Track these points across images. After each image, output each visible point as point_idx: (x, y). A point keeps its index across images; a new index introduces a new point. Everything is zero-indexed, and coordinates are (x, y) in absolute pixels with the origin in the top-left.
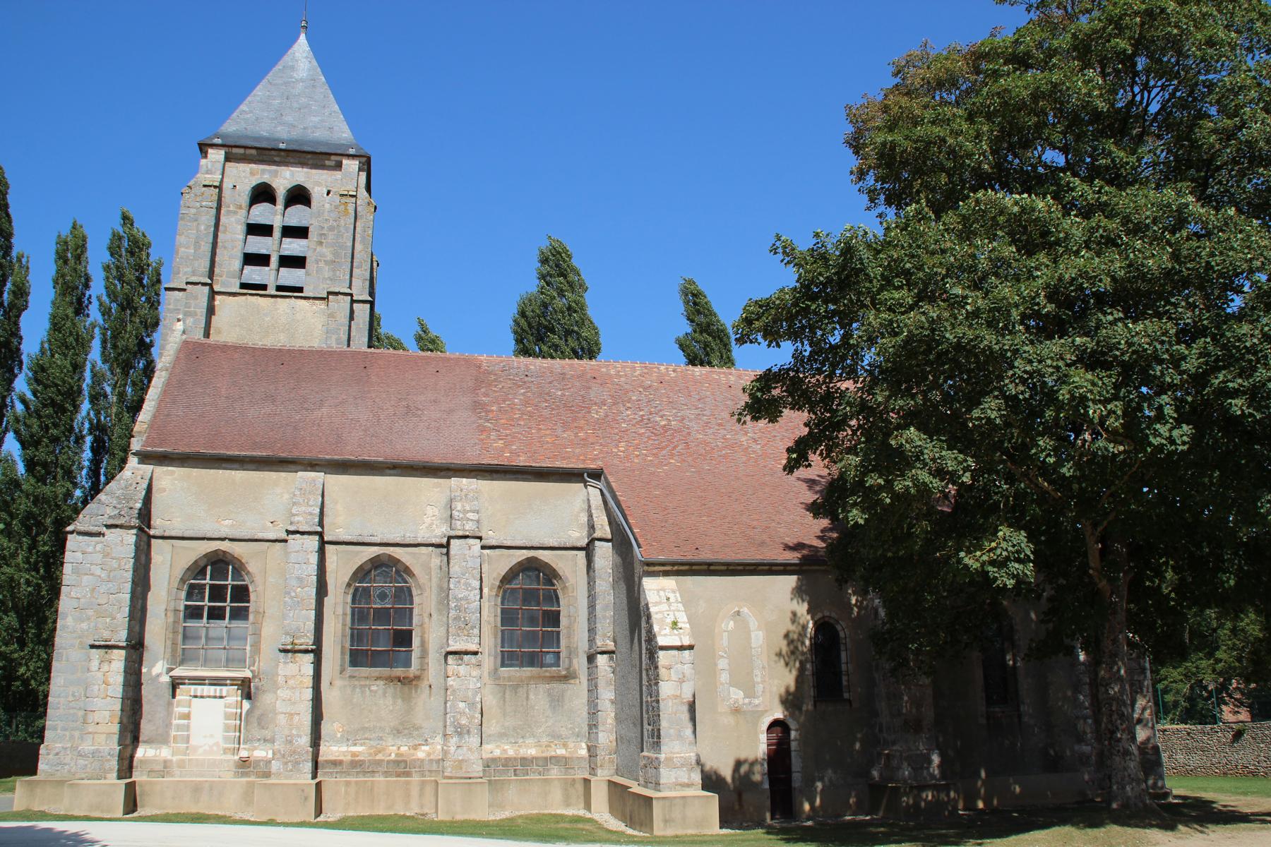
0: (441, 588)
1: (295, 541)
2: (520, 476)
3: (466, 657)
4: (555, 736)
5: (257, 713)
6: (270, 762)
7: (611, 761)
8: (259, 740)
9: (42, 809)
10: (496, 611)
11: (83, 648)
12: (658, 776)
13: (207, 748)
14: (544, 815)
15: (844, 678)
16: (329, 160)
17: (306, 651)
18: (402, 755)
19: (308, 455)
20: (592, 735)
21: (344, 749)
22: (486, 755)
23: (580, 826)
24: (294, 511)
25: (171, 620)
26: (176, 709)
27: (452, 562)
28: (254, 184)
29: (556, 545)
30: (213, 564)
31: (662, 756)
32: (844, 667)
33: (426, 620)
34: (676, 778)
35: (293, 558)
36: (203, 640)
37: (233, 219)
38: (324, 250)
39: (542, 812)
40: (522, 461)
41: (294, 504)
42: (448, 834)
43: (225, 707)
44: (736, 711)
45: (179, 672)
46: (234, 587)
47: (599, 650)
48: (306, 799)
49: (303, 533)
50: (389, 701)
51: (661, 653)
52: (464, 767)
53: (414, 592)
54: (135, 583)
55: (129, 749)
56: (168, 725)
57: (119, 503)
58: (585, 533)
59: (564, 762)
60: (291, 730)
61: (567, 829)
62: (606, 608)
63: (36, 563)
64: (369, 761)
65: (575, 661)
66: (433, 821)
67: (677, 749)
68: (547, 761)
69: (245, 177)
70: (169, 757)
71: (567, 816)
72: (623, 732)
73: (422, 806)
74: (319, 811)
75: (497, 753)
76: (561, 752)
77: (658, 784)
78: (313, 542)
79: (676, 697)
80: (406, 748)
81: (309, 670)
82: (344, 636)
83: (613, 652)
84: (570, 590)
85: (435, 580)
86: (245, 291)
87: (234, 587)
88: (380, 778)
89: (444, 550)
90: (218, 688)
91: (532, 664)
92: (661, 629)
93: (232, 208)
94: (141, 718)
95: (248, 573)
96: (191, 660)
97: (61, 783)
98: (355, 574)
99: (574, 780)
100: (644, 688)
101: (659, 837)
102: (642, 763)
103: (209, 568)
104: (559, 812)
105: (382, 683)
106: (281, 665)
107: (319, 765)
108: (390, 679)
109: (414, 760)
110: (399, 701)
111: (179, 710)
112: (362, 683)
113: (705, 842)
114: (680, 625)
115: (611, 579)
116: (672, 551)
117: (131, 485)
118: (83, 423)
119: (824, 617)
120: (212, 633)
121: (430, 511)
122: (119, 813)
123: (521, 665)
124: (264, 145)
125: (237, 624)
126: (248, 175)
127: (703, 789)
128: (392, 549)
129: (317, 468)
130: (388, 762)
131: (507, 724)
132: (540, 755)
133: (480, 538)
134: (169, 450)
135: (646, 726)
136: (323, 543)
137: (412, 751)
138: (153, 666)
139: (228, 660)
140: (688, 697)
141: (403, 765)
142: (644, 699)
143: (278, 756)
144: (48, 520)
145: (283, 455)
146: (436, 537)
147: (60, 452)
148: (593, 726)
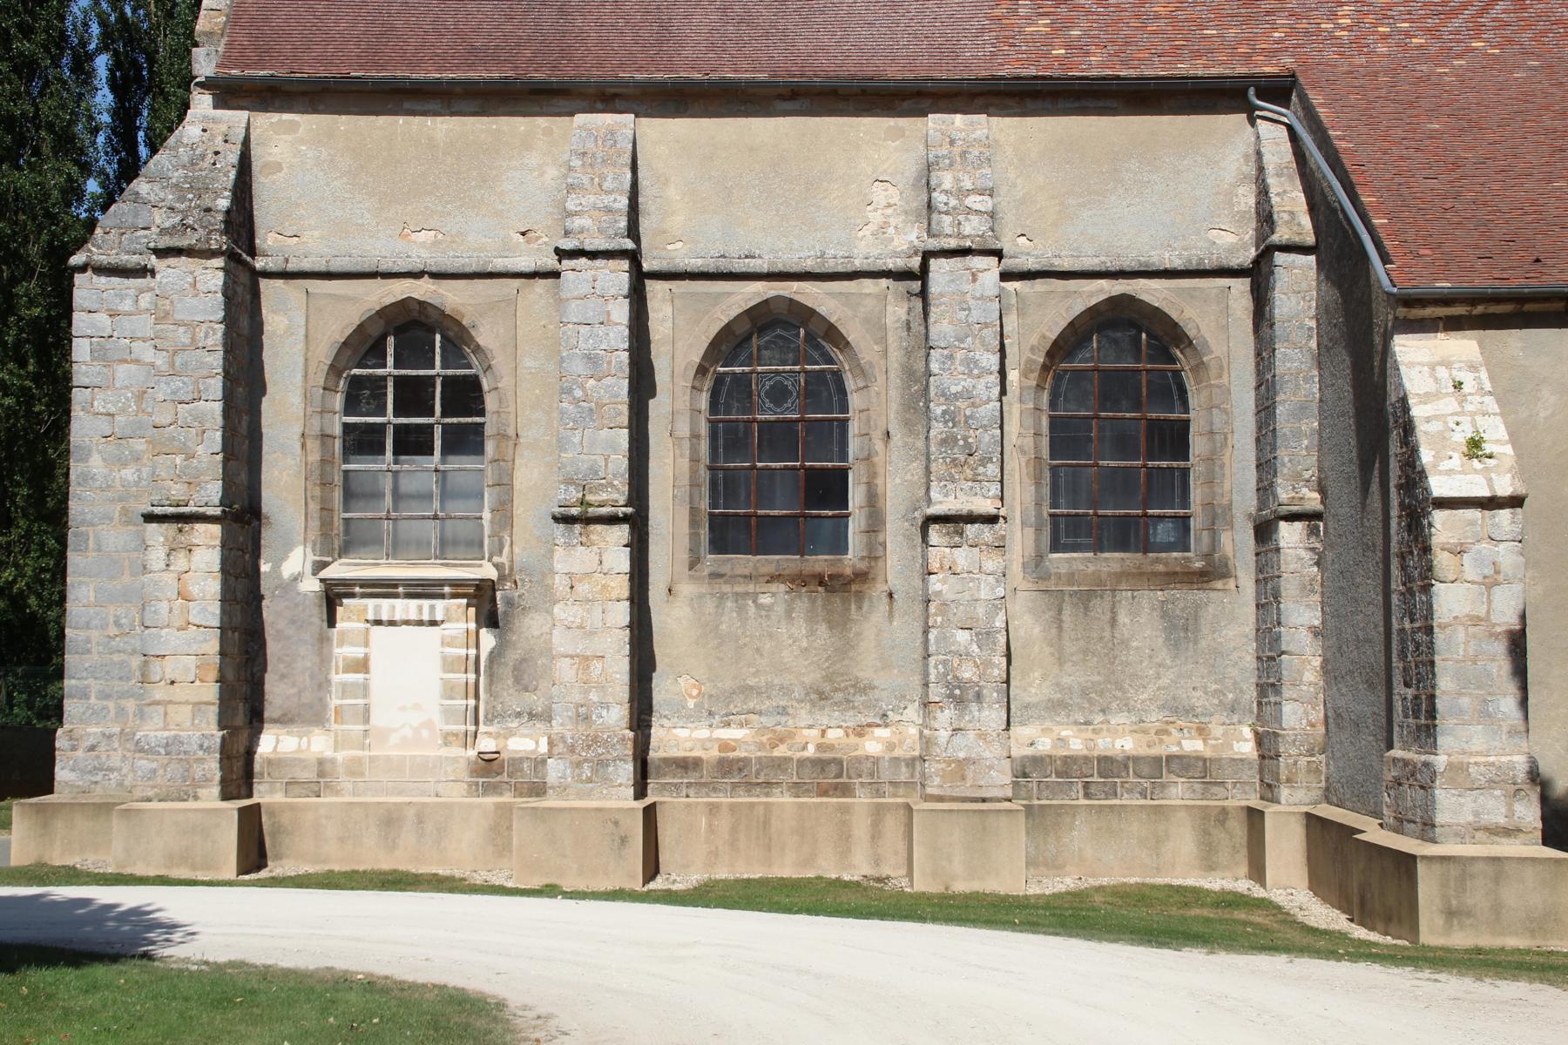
0: (909, 374)
1: (578, 275)
2: (1090, 103)
3: (971, 530)
4: (1178, 709)
5: (512, 656)
6: (544, 762)
7: (1313, 770)
8: (519, 715)
9: (70, 862)
10: (1038, 423)
11: (128, 523)
12: (1429, 806)
13: (408, 732)
14: (1153, 887)
17: (612, 520)
18: (831, 747)
19: (596, 74)
20: (1268, 710)
21: (704, 733)
22: (1018, 751)
23: (1241, 915)
24: (571, 206)
25: (315, 457)
26: (337, 650)
27: (933, 310)
29: (1178, 264)
30: (399, 331)
31: (1440, 761)
33: (879, 446)
34: (1476, 814)
35: (574, 311)
36: (388, 499)
39: (1148, 880)
40: (1095, 65)
41: (571, 188)
42: (935, 920)
43: (443, 644)
45: (337, 570)
46: (447, 381)
47: (1284, 510)
48: (624, 840)
49: (593, 255)
50: (800, 628)
51: (1439, 517)
52: (970, 775)
53: (850, 383)
54: (230, 378)
55: (244, 736)
56: (323, 685)
57: (182, 199)
58: (1249, 234)
59: (1201, 770)
60: (587, 692)
61: (1208, 920)
62: (1301, 411)
63: (18, 344)
64: (759, 759)
65: (1225, 539)
66: (901, 894)
67: (1478, 743)
68: (1160, 767)
70: (329, 753)
71: (1208, 892)
72: (1341, 703)
73: (877, 862)
74: (652, 868)
75: (1045, 746)
76: (1192, 746)
77: (1429, 824)
78: (616, 276)
79: (1476, 620)
80: (840, 733)
81: (620, 560)
82: (694, 484)
83: (1315, 516)
84: (1213, 372)
85: (895, 356)
89: (916, 286)
90: (426, 603)
91: (1122, 545)
92: (1438, 458)
94: (264, 670)
95: (478, 349)
96: (365, 543)
97: (104, 809)
98: (715, 344)
99: (1224, 811)
100: (1395, 599)
101: (1430, 949)
102: (1390, 774)
103: (391, 340)
104: (1190, 882)
105: (782, 588)
106: (559, 552)
107: (651, 769)
108: (801, 581)
109: (858, 760)
110: (822, 629)
111: (343, 652)
112: (739, 589)
113: (1553, 968)
114: (1488, 448)
115: (1313, 344)
116: (1472, 269)
117: (203, 157)
118: (86, 25)
120: (407, 485)
121: (880, 194)
122: (230, 870)
123: (1098, 547)
125: (460, 464)
127: (1546, 841)
128: (795, 285)
129: (618, 103)
130: (801, 763)
131: (1066, 680)
132: (1144, 751)
133: (998, 254)
134: (281, 73)
135: (1399, 688)
136: (639, 279)
137: (853, 739)
138: (284, 558)
139: (443, 543)
140: (1506, 616)
141: (833, 769)
142: (1395, 625)
143: (560, 748)
144: (34, 250)
146: (895, 254)
147: (41, 94)
148: (1269, 687)
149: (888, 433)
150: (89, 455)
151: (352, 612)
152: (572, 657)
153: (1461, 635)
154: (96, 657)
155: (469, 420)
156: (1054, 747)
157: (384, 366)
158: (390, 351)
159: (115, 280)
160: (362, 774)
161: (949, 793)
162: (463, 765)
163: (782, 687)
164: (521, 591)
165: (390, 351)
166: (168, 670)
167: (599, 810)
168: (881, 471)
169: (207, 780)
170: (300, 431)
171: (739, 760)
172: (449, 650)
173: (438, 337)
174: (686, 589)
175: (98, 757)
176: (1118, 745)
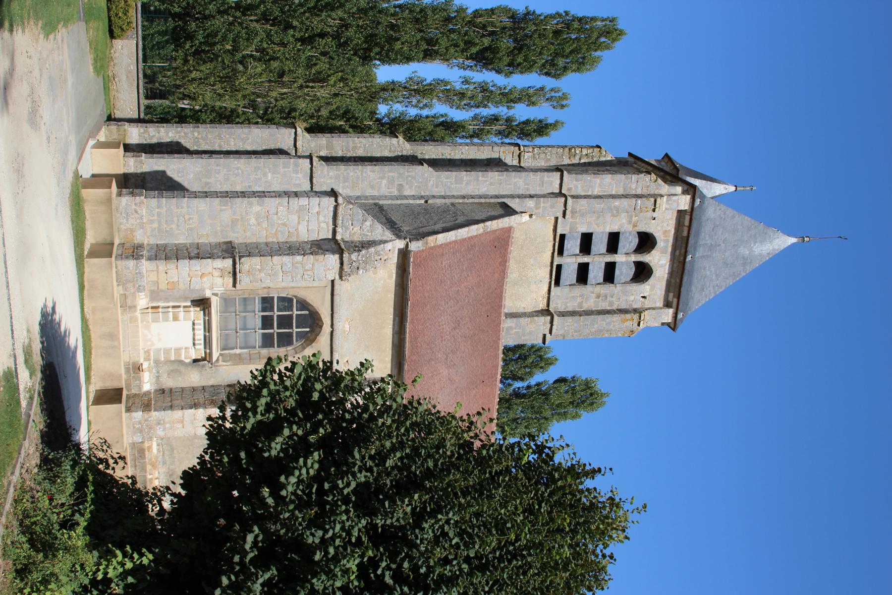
5: (182, 368)
8: (158, 372)
13: (149, 337)
16: (674, 296)
28: (656, 235)
37: (624, 221)
38: (592, 300)
43: (186, 348)
64: (145, 462)
70: (139, 308)
86: (557, 240)
90: (202, 342)
93: (634, 219)
103: (307, 312)
124: (691, 242)
126: (664, 229)
134: (411, 276)
145: (406, 367)
150: (260, 206)
151: (196, 314)
154: (175, 211)
155: (276, 342)
158: (303, 312)
159: (332, 214)
160: (131, 322)
163: (174, 462)
164: (208, 370)
165: (303, 312)
171: (145, 456)
172: (183, 351)
173: (308, 330)
175: (132, 214)
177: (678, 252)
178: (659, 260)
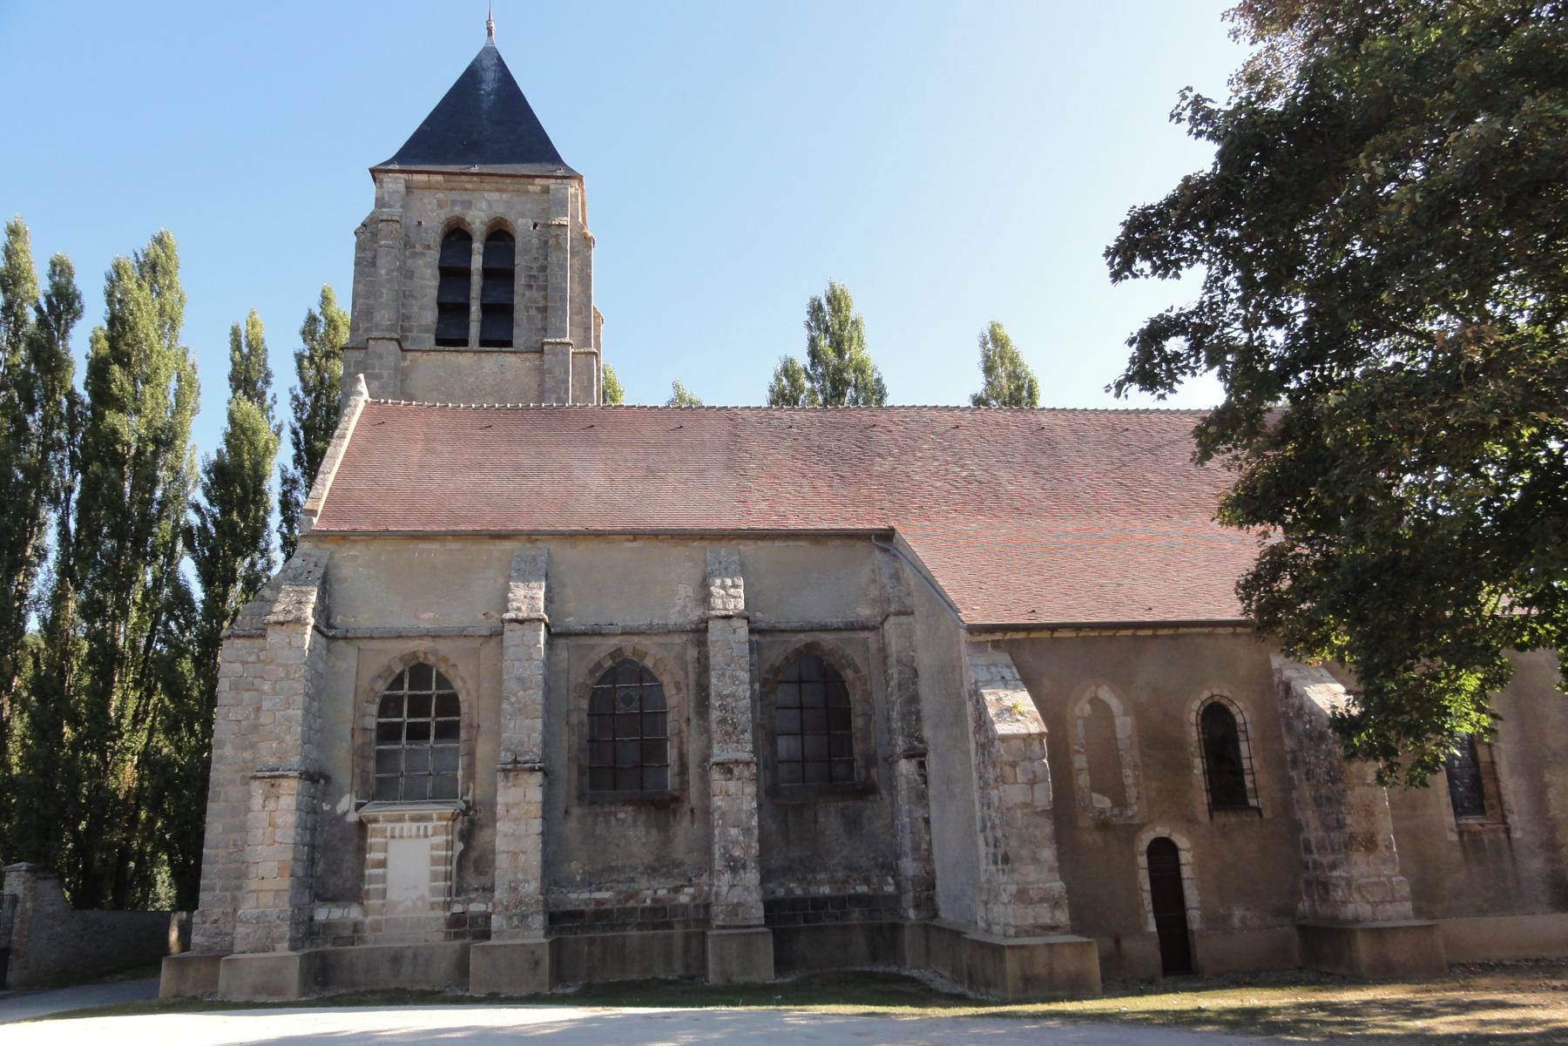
5: (474, 854)
8: (477, 890)
13: (410, 903)
15: (1248, 780)
16: (533, 184)
21: (586, 895)
26: (368, 856)
32: (1246, 764)
34: (1035, 918)
44: (1104, 825)
48: (537, 963)
50: (641, 831)
56: (361, 877)
60: (517, 873)
64: (618, 909)
69: (432, 211)
70: (360, 918)
75: (781, 892)
76: (862, 889)
79: (1026, 805)
87: (439, 697)
88: (632, 933)
104: (866, 969)
110: (654, 832)
117: (301, 574)
119: (1212, 696)
130: (644, 910)
132: (834, 894)
137: (672, 895)
138: (339, 801)
143: (500, 908)
149: (689, 719)
152: (507, 852)
153: (1019, 814)
156: (786, 893)
157: (402, 689)
161: (729, 924)
162: (442, 921)
163: (631, 866)
166: (260, 871)
167: (522, 945)
168: (685, 740)
169: (281, 938)
170: (351, 726)
174: (576, 811)
176: (821, 891)
177: (468, 186)
178: (481, 210)
